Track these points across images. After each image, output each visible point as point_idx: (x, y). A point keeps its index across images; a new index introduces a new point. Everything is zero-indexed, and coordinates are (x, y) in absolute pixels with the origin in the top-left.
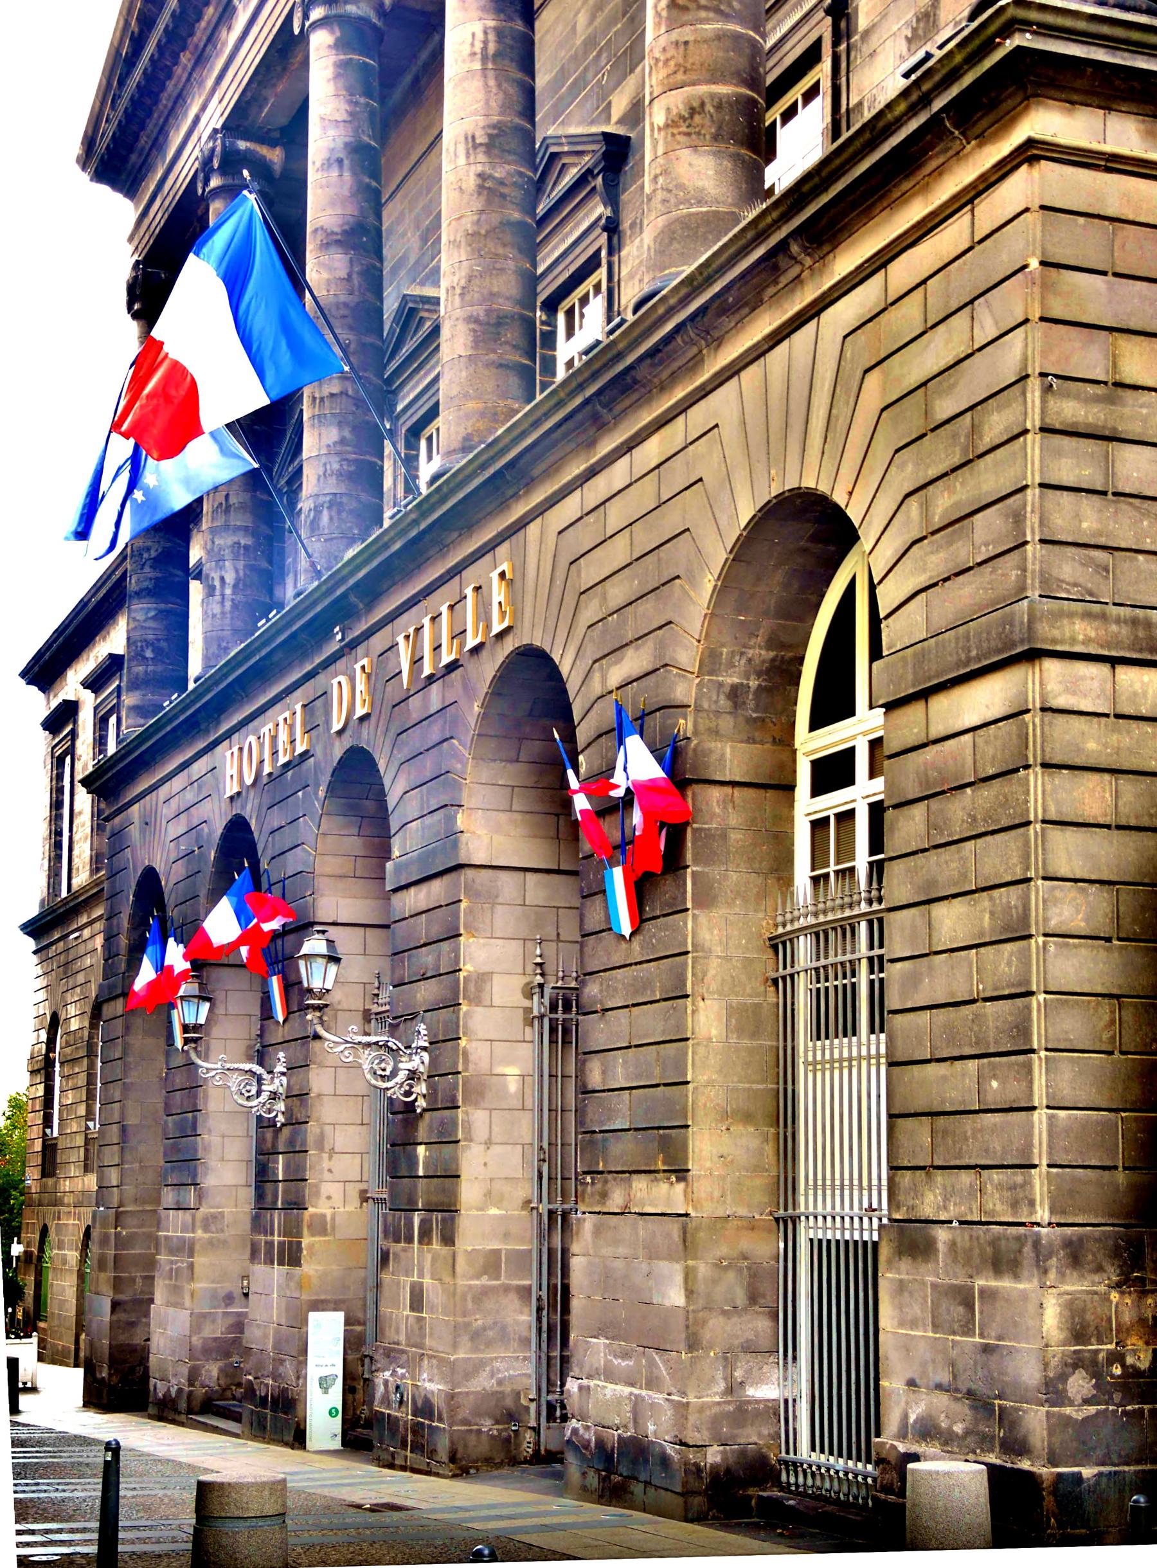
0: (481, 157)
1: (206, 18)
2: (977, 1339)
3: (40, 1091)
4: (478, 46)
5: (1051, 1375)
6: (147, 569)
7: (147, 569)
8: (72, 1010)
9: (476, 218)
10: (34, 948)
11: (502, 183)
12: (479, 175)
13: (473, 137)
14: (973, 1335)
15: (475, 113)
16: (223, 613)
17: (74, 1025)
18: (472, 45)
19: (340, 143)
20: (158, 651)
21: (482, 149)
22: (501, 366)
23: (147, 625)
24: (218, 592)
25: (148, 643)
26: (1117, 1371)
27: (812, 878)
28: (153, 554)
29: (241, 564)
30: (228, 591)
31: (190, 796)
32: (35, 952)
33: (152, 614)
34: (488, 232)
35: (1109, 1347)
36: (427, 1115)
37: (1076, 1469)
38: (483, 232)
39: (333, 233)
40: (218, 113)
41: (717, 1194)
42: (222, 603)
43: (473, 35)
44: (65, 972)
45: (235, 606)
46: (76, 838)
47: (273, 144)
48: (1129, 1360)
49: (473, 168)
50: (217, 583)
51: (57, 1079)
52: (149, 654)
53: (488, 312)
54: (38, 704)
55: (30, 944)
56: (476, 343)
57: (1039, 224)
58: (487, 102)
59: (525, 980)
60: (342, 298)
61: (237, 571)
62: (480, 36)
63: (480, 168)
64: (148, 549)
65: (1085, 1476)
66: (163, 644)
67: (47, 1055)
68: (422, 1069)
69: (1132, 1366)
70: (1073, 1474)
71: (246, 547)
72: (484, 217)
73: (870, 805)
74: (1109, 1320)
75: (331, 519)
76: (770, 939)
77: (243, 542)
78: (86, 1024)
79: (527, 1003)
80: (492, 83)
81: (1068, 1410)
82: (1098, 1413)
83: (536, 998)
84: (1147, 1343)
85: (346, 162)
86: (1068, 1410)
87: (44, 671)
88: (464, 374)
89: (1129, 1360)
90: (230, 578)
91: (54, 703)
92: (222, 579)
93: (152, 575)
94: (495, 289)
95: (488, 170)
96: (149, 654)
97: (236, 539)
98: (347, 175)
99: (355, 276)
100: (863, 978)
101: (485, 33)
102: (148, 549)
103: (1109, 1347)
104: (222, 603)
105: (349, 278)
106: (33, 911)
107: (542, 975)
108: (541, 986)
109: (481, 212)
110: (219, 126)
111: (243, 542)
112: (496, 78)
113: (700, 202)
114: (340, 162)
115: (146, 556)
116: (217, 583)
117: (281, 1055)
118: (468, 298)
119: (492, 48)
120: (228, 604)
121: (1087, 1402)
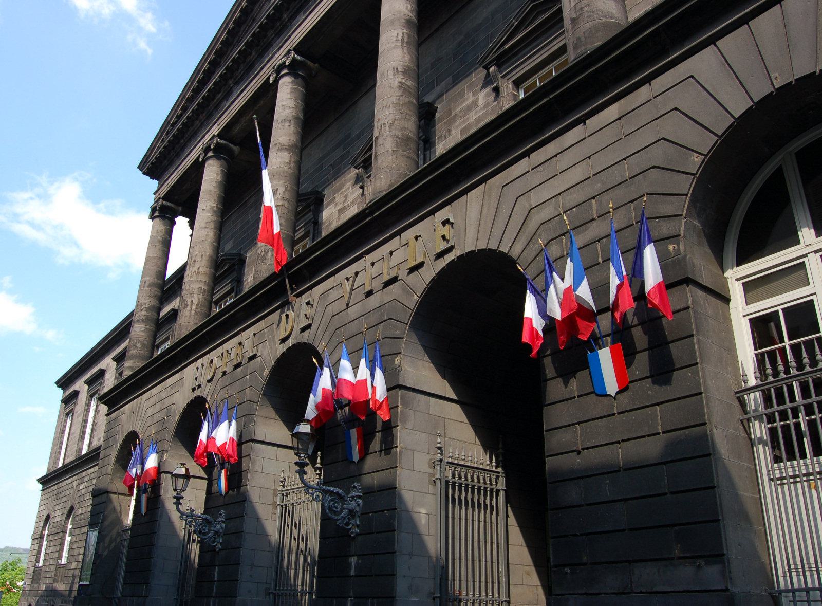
0: (400, 76)
1: (217, 98)
3: (36, 547)
4: (400, 38)
6: (143, 311)
7: (143, 311)
8: (58, 513)
9: (398, 98)
10: (41, 489)
11: (409, 87)
12: (400, 82)
13: (397, 69)
15: (201, 282)
16: (190, 316)
17: (58, 519)
18: (397, 37)
19: (290, 115)
20: (143, 344)
21: (401, 73)
22: (408, 157)
23: (140, 333)
24: (189, 307)
25: (139, 341)
27: (755, 354)
28: (147, 306)
29: (201, 297)
30: (194, 307)
31: (163, 395)
32: (42, 491)
33: (143, 329)
34: (403, 104)
36: (360, 538)
38: (401, 103)
39: (284, 145)
40: (217, 129)
42: (191, 311)
43: (398, 34)
44: (56, 497)
45: (196, 313)
46: (70, 443)
47: (235, 145)
49: (397, 79)
50: (189, 303)
51: (45, 543)
52: (139, 345)
53: (403, 134)
54: (59, 394)
55: (40, 486)
56: (397, 146)
58: (404, 57)
59: (428, 457)
60: (287, 170)
61: (199, 299)
62: (401, 35)
63: (400, 80)
64: (145, 304)
66: (145, 342)
67: (41, 532)
68: (357, 509)
71: (204, 290)
72: (401, 98)
73: (750, 320)
75: (272, 255)
76: (737, 393)
77: (203, 288)
78: (64, 518)
79: (431, 471)
80: (406, 51)
83: (437, 467)
85: (292, 122)
87: (64, 382)
88: (390, 158)
90: (195, 302)
91: (68, 393)
92: (192, 301)
93: (146, 314)
94: (406, 126)
95: (403, 80)
96: (139, 345)
97: (200, 286)
98: (292, 126)
99: (292, 162)
100: (802, 419)
101: (403, 34)
102: (145, 304)
104: (191, 311)
105: (289, 163)
106: (43, 472)
107: (442, 454)
108: (441, 460)
109: (400, 96)
110: (216, 134)
111: (203, 288)
112: (408, 50)
113: (611, 17)
114: (290, 121)
115: (144, 306)
116: (189, 303)
117: (222, 512)
118: (393, 128)
119: (406, 40)
120: (193, 312)
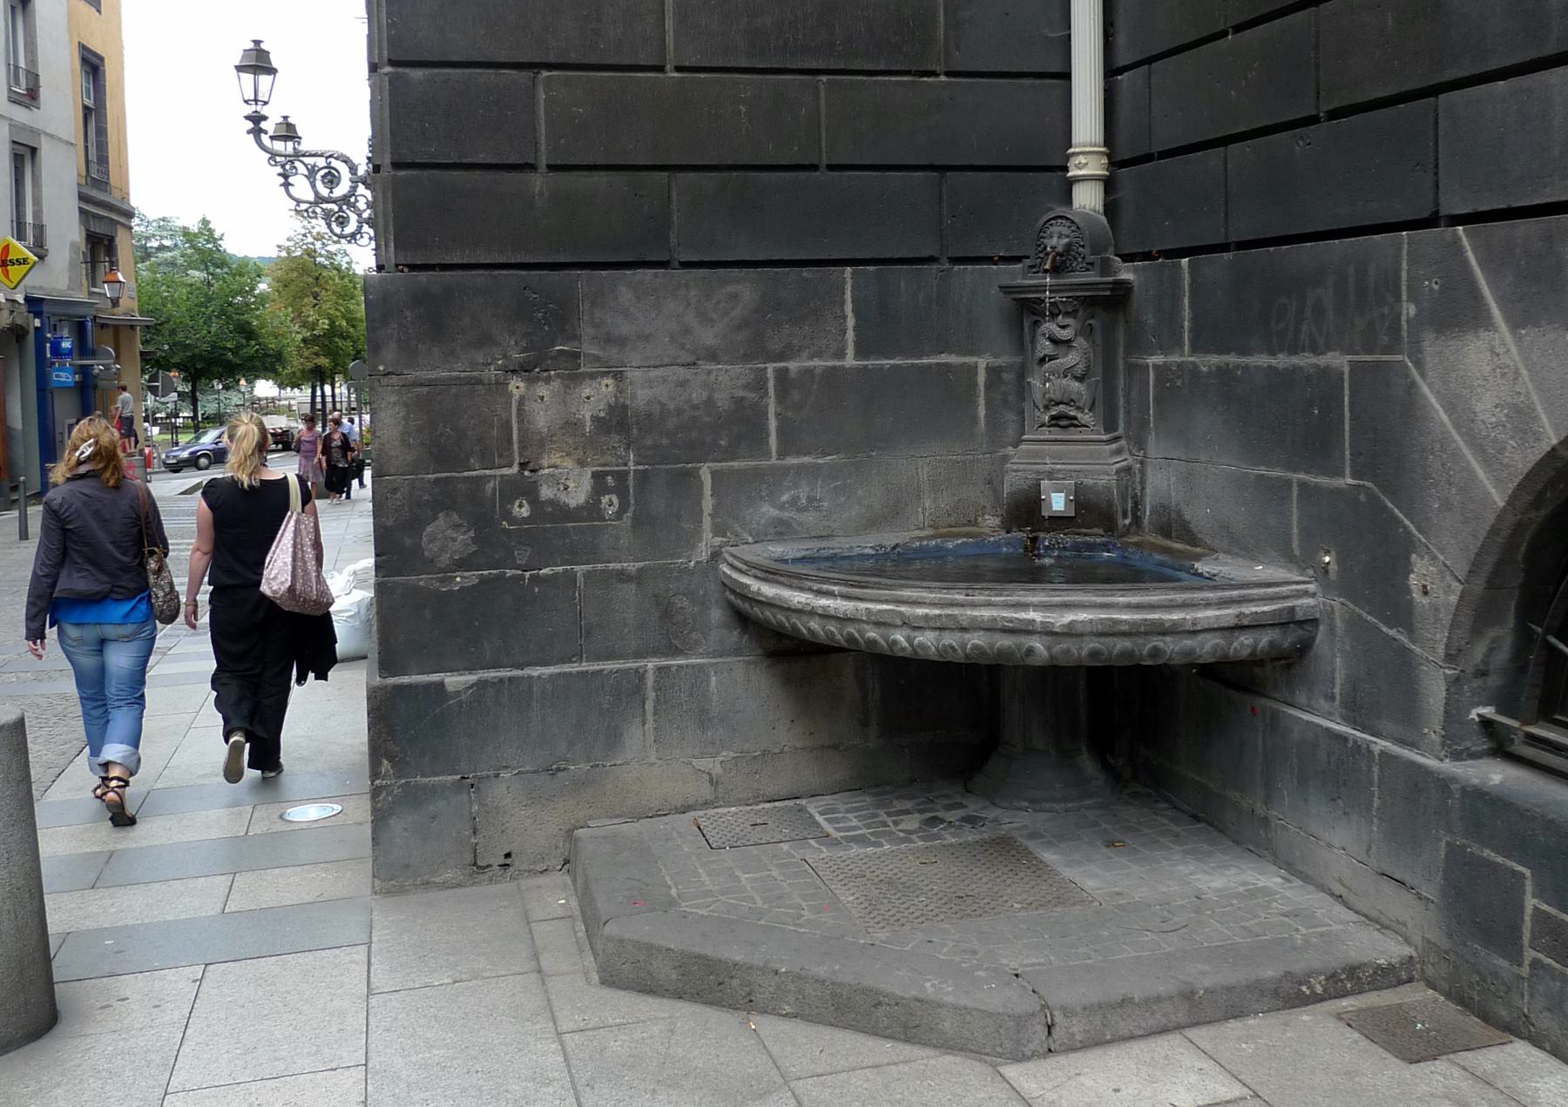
2: (1350, 481)
5: (390, 523)
14: (1341, 474)
26: (523, 510)
35: (506, 471)
37: (435, 677)
41: (1193, 1078)
48: (546, 492)
57: (76, 735)
65: (450, 688)
69: (552, 502)
70: (428, 685)
74: (507, 426)
81: (422, 580)
82: (484, 581)
84: (582, 463)
86: (422, 580)
89: (546, 492)
103: (506, 471)
121: (463, 564)
